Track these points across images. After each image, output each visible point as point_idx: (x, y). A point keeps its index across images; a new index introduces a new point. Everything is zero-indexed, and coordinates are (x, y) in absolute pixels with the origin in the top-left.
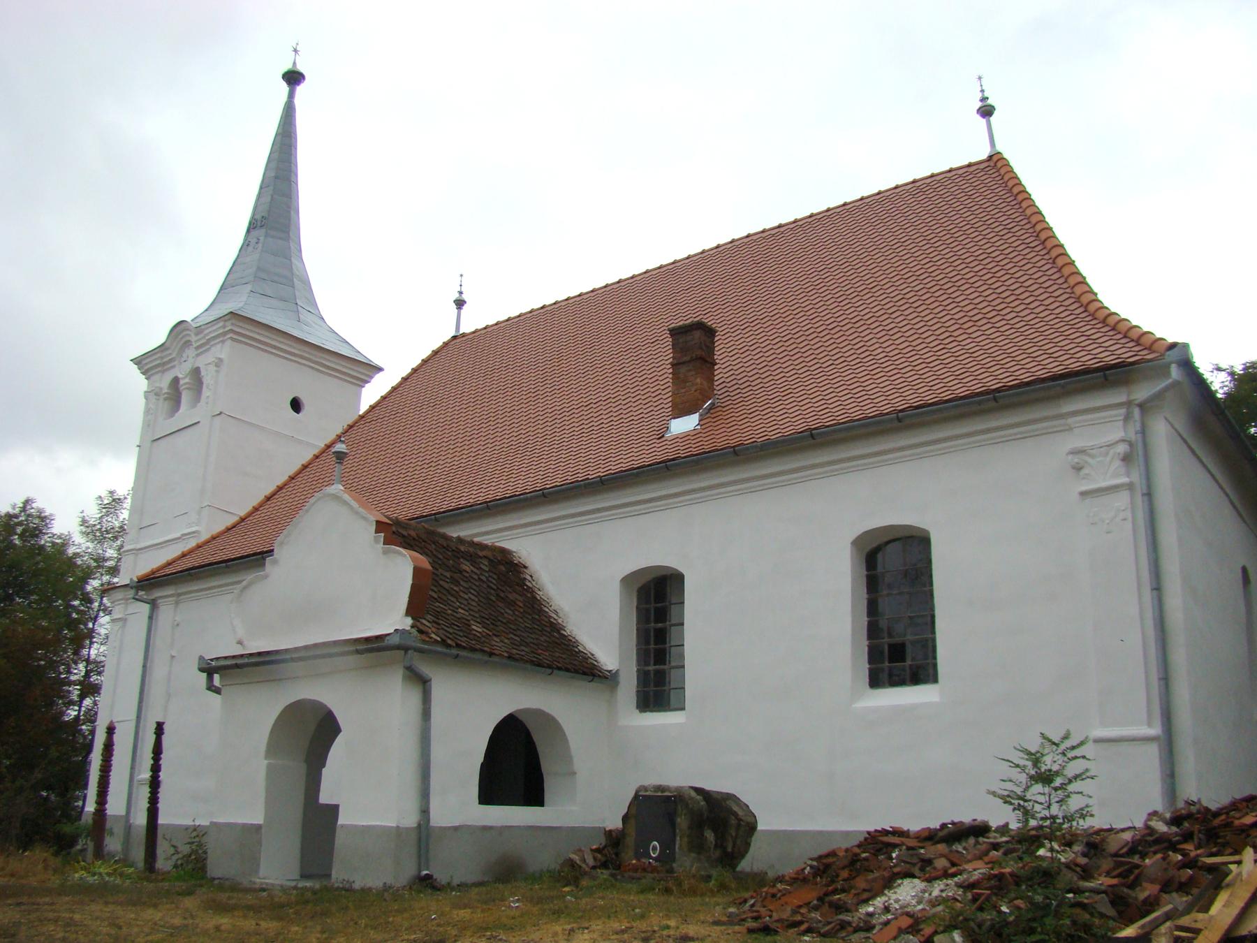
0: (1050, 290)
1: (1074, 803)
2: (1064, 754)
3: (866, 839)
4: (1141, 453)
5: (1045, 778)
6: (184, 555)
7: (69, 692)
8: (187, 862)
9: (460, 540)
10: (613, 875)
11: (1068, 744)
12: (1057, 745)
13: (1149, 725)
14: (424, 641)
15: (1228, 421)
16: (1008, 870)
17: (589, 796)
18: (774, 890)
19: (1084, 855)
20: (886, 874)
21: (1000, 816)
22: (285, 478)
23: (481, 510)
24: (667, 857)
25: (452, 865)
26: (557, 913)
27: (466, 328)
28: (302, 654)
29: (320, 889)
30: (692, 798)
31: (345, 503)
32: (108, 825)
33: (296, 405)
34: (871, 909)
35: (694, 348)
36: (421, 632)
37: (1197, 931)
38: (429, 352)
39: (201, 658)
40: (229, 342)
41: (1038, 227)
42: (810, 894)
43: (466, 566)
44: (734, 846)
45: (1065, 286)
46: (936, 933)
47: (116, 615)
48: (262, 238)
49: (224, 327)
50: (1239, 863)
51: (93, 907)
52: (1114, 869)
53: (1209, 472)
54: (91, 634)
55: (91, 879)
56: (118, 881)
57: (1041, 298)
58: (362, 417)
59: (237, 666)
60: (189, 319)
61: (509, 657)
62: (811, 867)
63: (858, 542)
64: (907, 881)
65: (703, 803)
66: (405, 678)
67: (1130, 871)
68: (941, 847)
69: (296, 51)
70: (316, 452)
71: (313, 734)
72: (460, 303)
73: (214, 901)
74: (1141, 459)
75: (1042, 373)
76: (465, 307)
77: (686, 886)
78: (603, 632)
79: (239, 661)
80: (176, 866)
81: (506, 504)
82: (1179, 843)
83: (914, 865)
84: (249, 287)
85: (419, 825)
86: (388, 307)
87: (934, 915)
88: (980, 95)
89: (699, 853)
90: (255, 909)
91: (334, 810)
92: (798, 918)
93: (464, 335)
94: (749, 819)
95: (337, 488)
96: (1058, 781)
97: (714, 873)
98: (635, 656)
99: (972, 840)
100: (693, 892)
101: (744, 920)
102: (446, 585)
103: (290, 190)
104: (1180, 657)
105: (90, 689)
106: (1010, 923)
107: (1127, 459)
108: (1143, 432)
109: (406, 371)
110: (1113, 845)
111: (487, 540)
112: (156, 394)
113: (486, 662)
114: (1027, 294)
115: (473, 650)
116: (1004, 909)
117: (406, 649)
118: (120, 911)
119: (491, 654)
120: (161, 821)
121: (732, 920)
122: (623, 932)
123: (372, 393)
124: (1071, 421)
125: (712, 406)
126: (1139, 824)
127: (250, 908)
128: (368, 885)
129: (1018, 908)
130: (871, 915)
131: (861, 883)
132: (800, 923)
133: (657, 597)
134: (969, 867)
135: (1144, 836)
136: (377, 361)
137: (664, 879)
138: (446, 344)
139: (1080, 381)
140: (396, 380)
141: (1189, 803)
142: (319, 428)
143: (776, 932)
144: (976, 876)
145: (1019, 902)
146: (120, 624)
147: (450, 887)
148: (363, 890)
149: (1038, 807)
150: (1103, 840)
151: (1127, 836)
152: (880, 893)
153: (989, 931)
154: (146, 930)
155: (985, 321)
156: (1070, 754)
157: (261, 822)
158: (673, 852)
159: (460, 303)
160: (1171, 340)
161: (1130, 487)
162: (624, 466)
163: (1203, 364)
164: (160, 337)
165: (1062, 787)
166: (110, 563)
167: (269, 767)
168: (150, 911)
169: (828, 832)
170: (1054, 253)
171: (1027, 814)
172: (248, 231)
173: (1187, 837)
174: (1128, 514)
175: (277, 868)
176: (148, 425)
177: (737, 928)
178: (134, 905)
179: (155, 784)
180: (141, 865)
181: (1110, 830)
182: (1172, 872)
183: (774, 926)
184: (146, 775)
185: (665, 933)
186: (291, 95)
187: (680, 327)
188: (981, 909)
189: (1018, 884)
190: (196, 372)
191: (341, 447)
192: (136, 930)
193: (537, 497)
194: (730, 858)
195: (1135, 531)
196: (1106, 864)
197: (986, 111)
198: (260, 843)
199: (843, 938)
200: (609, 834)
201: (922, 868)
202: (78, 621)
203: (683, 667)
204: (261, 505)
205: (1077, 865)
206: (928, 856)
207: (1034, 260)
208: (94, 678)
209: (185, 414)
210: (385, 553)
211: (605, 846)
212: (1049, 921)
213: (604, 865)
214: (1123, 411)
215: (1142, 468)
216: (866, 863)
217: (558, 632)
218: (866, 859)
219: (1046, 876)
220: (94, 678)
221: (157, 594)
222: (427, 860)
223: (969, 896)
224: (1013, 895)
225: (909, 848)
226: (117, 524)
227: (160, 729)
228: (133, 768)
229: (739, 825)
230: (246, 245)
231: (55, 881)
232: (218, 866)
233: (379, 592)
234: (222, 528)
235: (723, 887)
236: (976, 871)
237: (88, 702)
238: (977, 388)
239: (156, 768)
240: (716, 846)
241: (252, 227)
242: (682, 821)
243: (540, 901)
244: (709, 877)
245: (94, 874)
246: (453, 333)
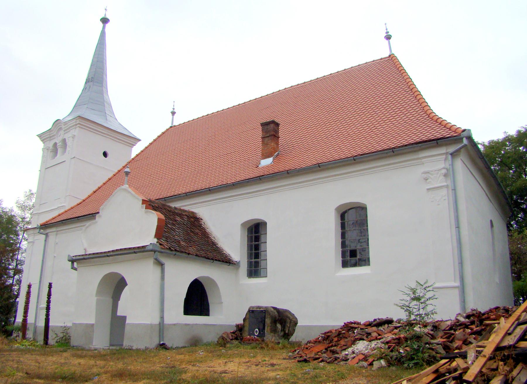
0: (414, 108)
1: (429, 308)
2: (425, 289)
4: (451, 173)
5: (418, 299)
6: (59, 215)
7: (9, 272)
8: (62, 340)
9: (176, 208)
10: (240, 342)
11: (427, 285)
12: (422, 286)
13: (455, 281)
14: (162, 248)
15: (486, 162)
16: (402, 336)
19: (432, 330)
21: (398, 315)
22: (101, 184)
23: (184, 196)
24: (262, 334)
25: (173, 340)
26: (219, 356)
27: (176, 123)
28: (112, 254)
29: (118, 350)
30: (272, 311)
31: (130, 192)
32: (28, 326)
33: (105, 154)
34: (347, 353)
35: (271, 130)
36: (160, 244)
38: (156, 137)
39: (69, 256)
40: (78, 128)
41: (409, 84)
42: (321, 347)
43: (178, 218)
45: (420, 107)
46: (374, 361)
47: (29, 241)
49: (76, 122)
50: (499, 323)
51: (27, 356)
52: (444, 335)
53: (477, 181)
54: (19, 249)
55: (22, 347)
57: (411, 112)
58: (133, 159)
59: (84, 259)
60: (61, 119)
61: (196, 255)
62: (322, 337)
63: (337, 209)
64: (361, 341)
65: (276, 313)
66: (154, 263)
67: (450, 336)
68: (374, 328)
69: (106, 10)
70: (114, 173)
71: (117, 286)
72: (173, 113)
74: (451, 176)
76: (175, 115)
77: (270, 346)
78: (234, 245)
79: (85, 257)
80: (57, 342)
81: (198, 193)
82: (469, 325)
84: (86, 106)
86: (144, 113)
88: (385, 31)
89: (275, 333)
90: (94, 357)
91: (124, 318)
92: (317, 356)
93: (175, 126)
94: (294, 320)
95: (126, 186)
97: (281, 341)
99: (386, 325)
100: (273, 348)
103: (103, 66)
104: (467, 254)
105: (18, 271)
107: (445, 175)
108: (452, 165)
109: (151, 141)
110: (443, 326)
111: (186, 208)
112: (47, 149)
113: (187, 257)
114: (405, 110)
116: (401, 351)
118: (38, 357)
119: (189, 254)
120: (50, 324)
121: (290, 358)
122: (247, 362)
123: (136, 150)
124: (423, 160)
125: (278, 155)
126: (453, 318)
127: (92, 356)
128: (139, 348)
129: (406, 350)
130: (347, 355)
131: (342, 342)
133: (255, 232)
134: (386, 336)
136: (138, 137)
137: (260, 342)
138: (168, 130)
140: (147, 144)
141: (472, 310)
142: (115, 164)
143: (309, 361)
145: (408, 349)
146: (31, 244)
148: (137, 349)
149: (414, 310)
150: (439, 325)
151: (449, 323)
152: (351, 346)
153: (395, 360)
154: (50, 364)
156: (428, 289)
159: (173, 113)
160: (463, 128)
161: (447, 186)
162: (242, 179)
163: (477, 138)
164: (49, 126)
165: (424, 302)
166: (28, 220)
167: (97, 299)
168: (51, 357)
170: (416, 94)
171: (410, 313)
172: (86, 83)
173: (473, 323)
174: (446, 198)
175: (100, 341)
176: (44, 162)
177: (293, 360)
178: (44, 355)
179: (48, 308)
182: (467, 336)
183: (308, 359)
184: (45, 305)
185: (264, 362)
186: (104, 28)
187: (265, 123)
188: (392, 351)
189: (406, 341)
190: (64, 141)
191: (127, 170)
192: (46, 364)
193: (207, 191)
194: (287, 336)
196: (441, 334)
197: (388, 37)
198: (93, 331)
199: (336, 364)
202: (13, 243)
203: (266, 260)
205: (429, 334)
206: (369, 332)
208: (19, 267)
209: (60, 157)
210: (146, 212)
212: (420, 354)
213: (236, 339)
214: (444, 156)
215: (452, 178)
216: (344, 335)
218: (344, 333)
219: (418, 338)
220: (19, 267)
221: (48, 231)
222: (163, 337)
223: (387, 346)
224: (405, 345)
225: (361, 329)
226: (31, 204)
227: (50, 286)
228: (38, 302)
231: (6, 347)
232: (74, 342)
233: (144, 228)
234: (76, 204)
235: (284, 347)
236: (389, 337)
237: (17, 277)
238: (386, 147)
239: (49, 302)
241: (87, 81)
242: (268, 321)
243: (211, 352)
244: (279, 343)
245: (23, 345)
246: (170, 125)
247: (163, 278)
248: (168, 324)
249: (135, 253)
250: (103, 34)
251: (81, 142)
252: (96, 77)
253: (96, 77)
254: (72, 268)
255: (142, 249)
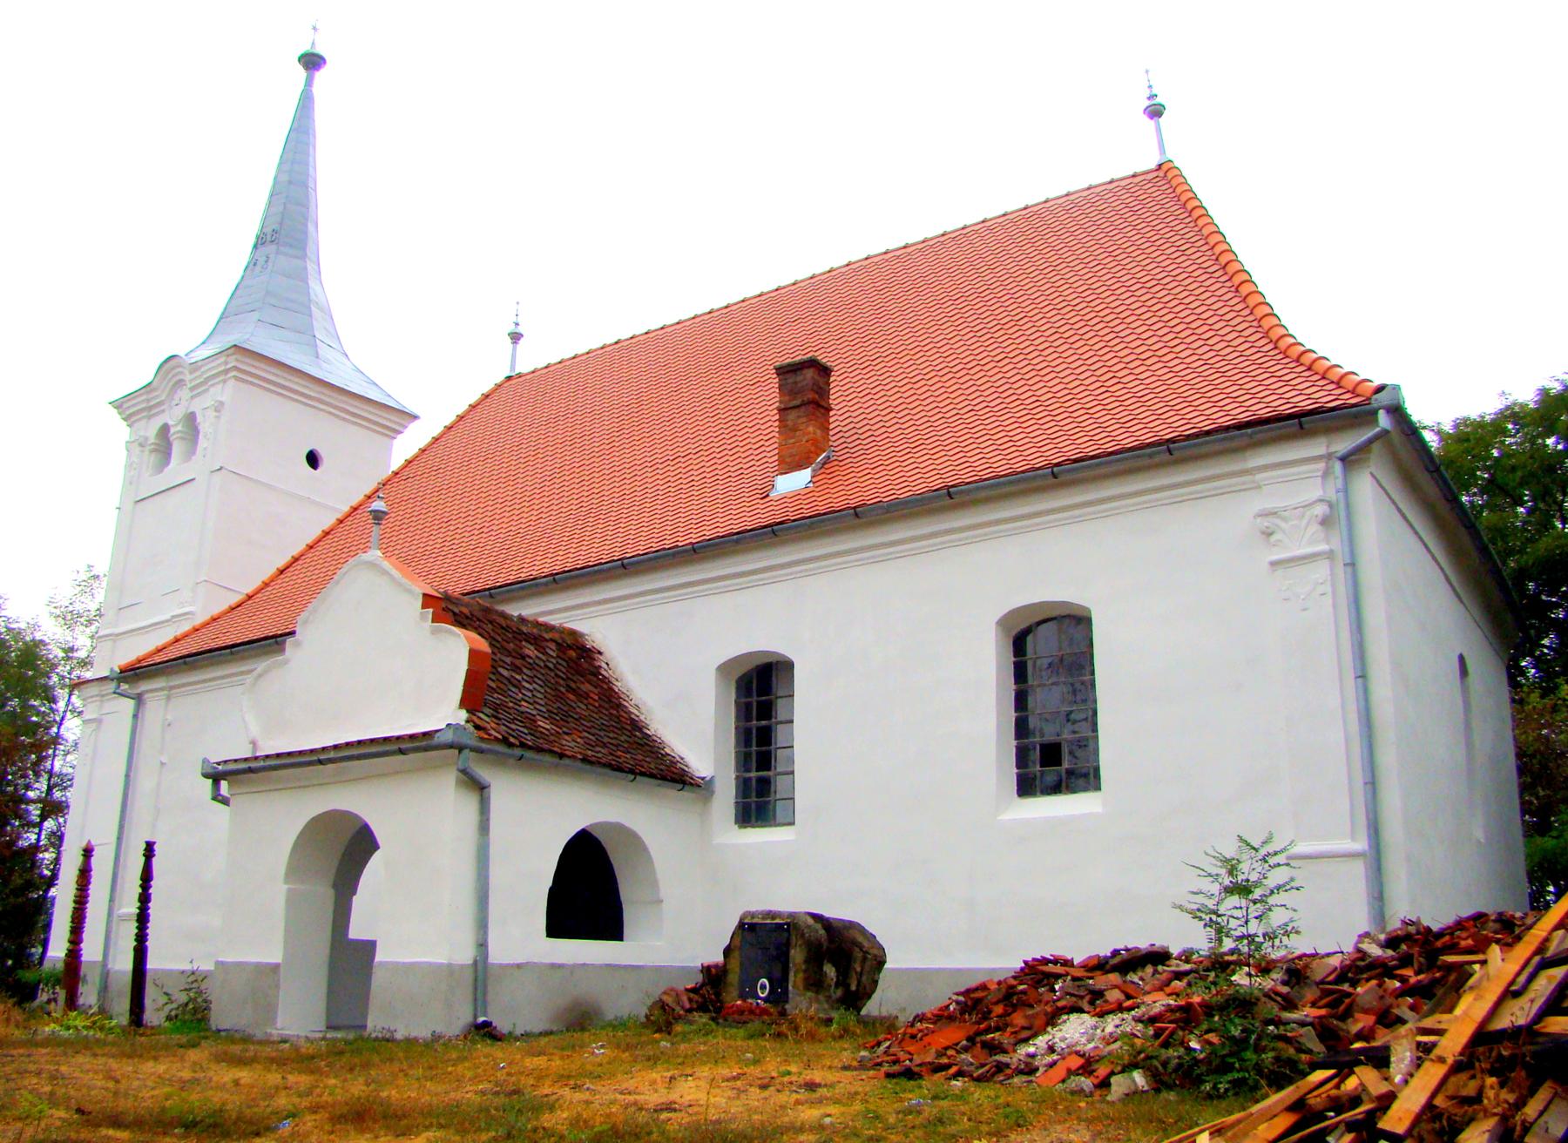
1: (1277, 918)
3: (1022, 969)
4: (1342, 514)
5: (1243, 889)
6: (177, 640)
7: (27, 811)
8: (184, 1013)
9: (522, 620)
10: (713, 1019)
11: (1270, 848)
12: (1256, 850)
13: (1353, 838)
14: (482, 739)
15: (1445, 481)
16: (1196, 999)
17: (681, 922)
18: (914, 1030)
19: (1284, 983)
20: (1049, 1009)
21: (1186, 937)
22: (301, 547)
23: (546, 584)
24: (779, 996)
25: (516, 1011)
26: (653, 1060)
27: (524, 367)
28: (332, 755)
29: (351, 1041)
31: (385, 573)
32: (84, 970)
33: (313, 459)
34: (1032, 1049)
35: (806, 388)
36: (477, 727)
37: (1440, 1032)
39: (205, 761)
40: (232, 383)
41: (1218, 250)
44: (858, 985)
45: (1250, 318)
46: (1112, 1073)
47: (87, 716)
48: (272, 257)
49: (226, 363)
51: (80, 1059)
52: (1321, 998)
54: (56, 740)
55: (65, 1034)
56: (99, 1035)
59: (251, 770)
60: (182, 354)
62: (958, 1002)
63: (1004, 622)
64: (1073, 1016)
65: (822, 932)
66: (459, 783)
68: (1114, 978)
70: (339, 516)
71: (348, 850)
72: (516, 337)
73: (226, 1053)
74: (1343, 522)
75: (1225, 421)
77: (803, 1031)
78: (696, 730)
79: (253, 765)
80: (169, 1018)
83: (1082, 997)
84: (256, 315)
85: (475, 962)
86: (429, 338)
87: (1110, 1053)
90: (280, 1062)
91: (369, 947)
92: (945, 1060)
93: (520, 376)
94: (875, 951)
95: (375, 554)
96: (1257, 893)
97: (835, 1015)
98: (733, 762)
99: (1149, 969)
100: (812, 1037)
101: (880, 1064)
102: (505, 673)
103: (307, 196)
104: (1388, 757)
105: (54, 808)
106: (1201, 1061)
107: (1325, 522)
108: (1346, 490)
110: (1319, 971)
111: (554, 620)
112: (141, 445)
114: (1206, 328)
115: (539, 750)
116: (1194, 1044)
117: (461, 748)
118: (113, 1063)
119: (561, 756)
120: (150, 965)
121: (862, 1066)
124: (1259, 477)
125: (827, 460)
126: (1348, 948)
127: (272, 1060)
128: (413, 1034)
129: (1209, 1043)
130: (1032, 1056)
131: (1019, 1019)
132: (946, 1067)
133: (760, 690)
134: (1148, 999)
135: (1354, 961)
136: (411, 408)
137: (774, 1019)
139: (1271, 430)
142: (342, 487)
144: (1157, 1008)
145: (1213, 1037)
146: (94, 726)
147: (509, 1038)
149: (1233, 923)
150: (1306, 966)
151: (1335, 961)
152: (1042, 1030)
154: (150, 1084)
155: (1155, 359)
156: (1272, 861)
157: (279, 960)
158: (786, 991)
159: (516, 337)
161: (1330, 555)
162: (721, 531)
165: (1262, 900)
166: (82, 654)
167: (289, 890)
168: (151, 1063)
169: (969, 970)
171: (1221, 932)
172: (256, 247)
173: (1405, 961)
174: (1328, 589)
175: (299, 1016)
176: (130, 482)
178: (130, 1057)
179: (143, 918)
180: (124, 1019)
181: (1315, 955)
183: (916, 1069)
184: (133, 908)
185: (786, 1079)
186: (309, 82)
188: (1166, 1045)
190: (191, 419)
191: (378, 505)
192: (136, 1083)
194: (854, 999)
195: (1334, 606)
196: (1311, 993)
198: (277, 986)
200: (706, 970)
201: (1094, 1003)
202: (38, 725)
203: (792, 773)
204: (273, 579)
207: (1182, 315)
208: (57, 794)
209: (177, 469)
210: (434, 632)
211: (703, 985)
212: (1249, 1055)
213: (702, 1008)
214: (1321, 465)
215: (1345, 533)
217: (640, 730)
218: (1023, 992)
219: (1243, 1004)
220: (57, 794)
221: (144, 686)
222: (485, 1002)
223: (1151, 1031)
224: (1204, 1026)
225: (1074, 979)
227: (150, 850)
228: (112, 900)
229: (865, 959)
230: (253, 264)
231: (18, 1034)
232: (221, 1018)
233: (428, 679)
234: (225, 606)
235: (845, 1032)
236: (1158, 1002)
237: (50, 824)
238: (1148, 438)
239: (145, 899)
240: (837, 985)
241: (260, 242)
242: (797, 955)
243: (628, 1047)
244: (829, 1021)
245: (68, 1028)
247: (484, 827)
248: (501, 966)
249: (401, 752)
250: (306, 102)
251: (242, 424)
252: (286, 232)
253: (286, 232)
254: (214, 798)
255: (421, 743)
